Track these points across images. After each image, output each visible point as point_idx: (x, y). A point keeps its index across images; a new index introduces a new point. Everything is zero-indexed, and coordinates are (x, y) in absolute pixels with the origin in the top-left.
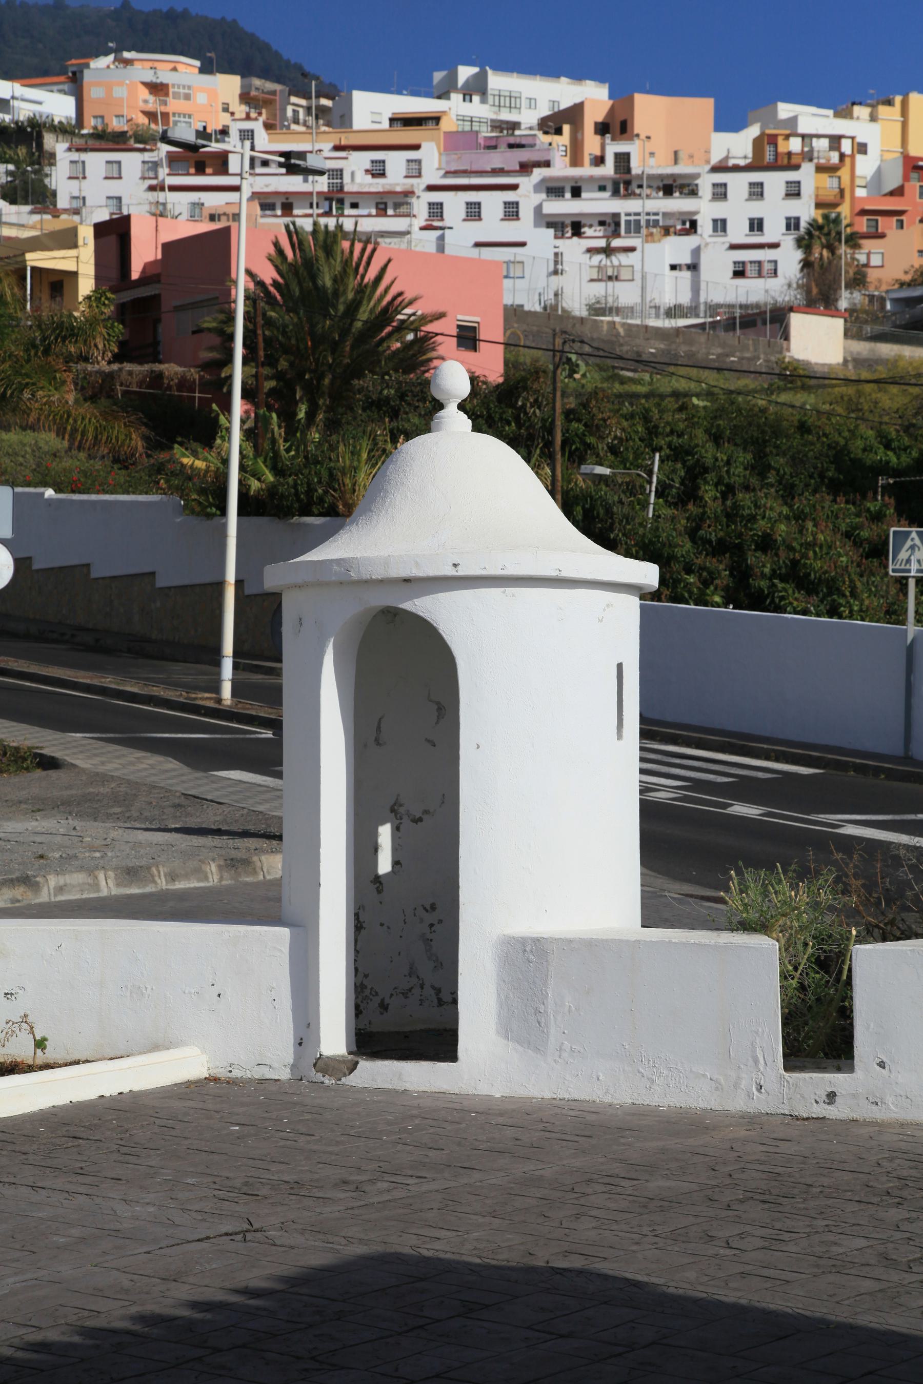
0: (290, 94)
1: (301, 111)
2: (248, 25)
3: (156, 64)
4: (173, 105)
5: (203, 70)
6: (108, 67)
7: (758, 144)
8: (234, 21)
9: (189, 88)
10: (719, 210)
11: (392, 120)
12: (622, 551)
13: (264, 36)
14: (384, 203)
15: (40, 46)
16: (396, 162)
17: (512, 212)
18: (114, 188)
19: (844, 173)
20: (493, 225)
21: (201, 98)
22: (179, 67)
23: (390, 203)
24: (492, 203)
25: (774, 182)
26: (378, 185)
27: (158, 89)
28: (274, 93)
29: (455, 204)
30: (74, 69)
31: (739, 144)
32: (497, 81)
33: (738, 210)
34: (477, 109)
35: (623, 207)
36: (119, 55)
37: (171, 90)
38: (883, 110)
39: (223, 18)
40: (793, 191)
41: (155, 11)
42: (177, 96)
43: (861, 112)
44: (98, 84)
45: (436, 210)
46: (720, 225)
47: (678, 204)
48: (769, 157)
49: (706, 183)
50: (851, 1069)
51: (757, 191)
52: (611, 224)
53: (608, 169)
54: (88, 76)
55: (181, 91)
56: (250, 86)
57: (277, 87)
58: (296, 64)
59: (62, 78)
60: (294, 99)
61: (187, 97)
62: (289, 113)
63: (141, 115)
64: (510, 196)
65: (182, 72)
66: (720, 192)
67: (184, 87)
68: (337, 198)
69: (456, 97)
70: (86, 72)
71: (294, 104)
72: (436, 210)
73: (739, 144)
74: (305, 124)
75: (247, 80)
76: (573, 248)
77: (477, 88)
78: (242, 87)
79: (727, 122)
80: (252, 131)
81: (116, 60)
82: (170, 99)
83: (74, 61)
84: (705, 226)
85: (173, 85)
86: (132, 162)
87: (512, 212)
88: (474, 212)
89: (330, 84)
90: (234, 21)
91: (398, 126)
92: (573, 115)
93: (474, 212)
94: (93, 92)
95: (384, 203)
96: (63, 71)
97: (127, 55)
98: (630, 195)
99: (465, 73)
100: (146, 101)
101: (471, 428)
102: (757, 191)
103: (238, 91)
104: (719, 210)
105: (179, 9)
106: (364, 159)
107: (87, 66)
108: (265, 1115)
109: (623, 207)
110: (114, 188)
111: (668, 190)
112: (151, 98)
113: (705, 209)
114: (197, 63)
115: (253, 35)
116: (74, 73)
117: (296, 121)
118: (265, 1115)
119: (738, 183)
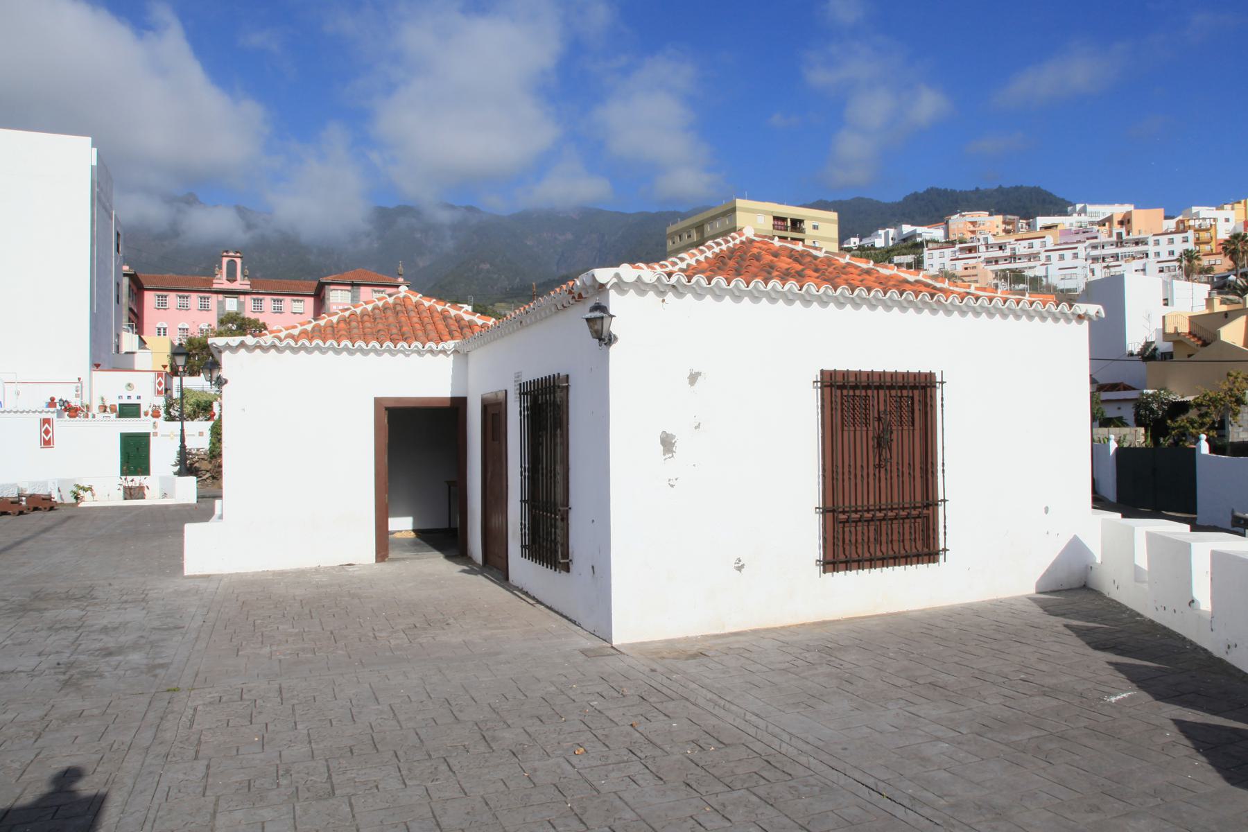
2: (1043, 188)
7: (1178, 223)
10: (1157, 249)
13: (1049, 190)
16: (1037, 243)
17: (1076, 256)
18: (942, 260)
19: (1212, 231)
20: (1069, 261)
23: (1033, 257)
24: (1068, 254)
25: (1178, 238)
26: (1030, 251)
31: (1171, 224)
32: (1090, 208)
34: (1083, 218)
38: (1236, 206)
43: (1228, 207)
45: (1048, 258)
46: (1157, 254)
47: (1141, 248)
48: (1181, 229)
49: (1151, 240)
50: (122, 434)
51: (1171, 241)
52: (1116, 257)
53: (1114, 238)
65: (982, 217)
66: (1157, 243)
68: (1014, 257)
69: (1075, 215)
72: (1048, 258)
73: (1171, 224)
77: (1084, 211)
84: (1151, 255)
87: (1076, 256)
88: (1062, 257)
92: (1109, 219)
93: (1062, 257)
94: (952, 226)
98: (1122, 246)
99: (1079, 206)
101: (830, 367)
104: (1157, 249)
106: (1026, 243)
110: (942, 260)
111: (1137, 244)
113: (1151, 249)
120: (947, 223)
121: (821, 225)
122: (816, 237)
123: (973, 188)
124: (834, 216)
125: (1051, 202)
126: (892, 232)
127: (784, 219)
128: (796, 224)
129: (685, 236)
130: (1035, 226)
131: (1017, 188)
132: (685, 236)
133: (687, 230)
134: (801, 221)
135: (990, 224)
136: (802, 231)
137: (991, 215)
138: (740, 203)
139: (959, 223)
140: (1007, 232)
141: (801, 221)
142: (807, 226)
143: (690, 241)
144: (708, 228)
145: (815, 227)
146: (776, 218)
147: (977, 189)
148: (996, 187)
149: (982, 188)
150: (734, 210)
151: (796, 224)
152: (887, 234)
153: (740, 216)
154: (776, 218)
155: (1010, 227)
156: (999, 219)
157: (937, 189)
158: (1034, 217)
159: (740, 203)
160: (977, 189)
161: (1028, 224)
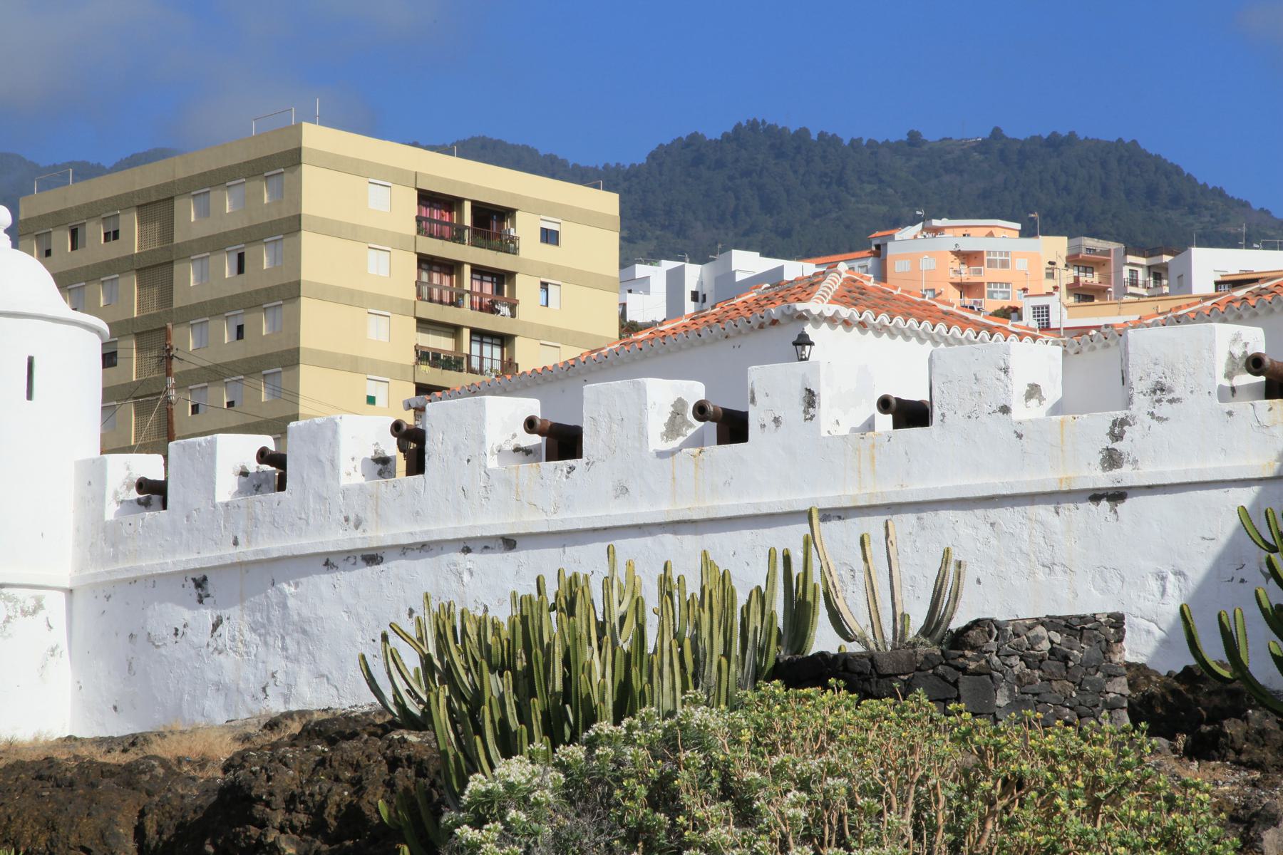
0: (1126, 254)
1: (1140, 271)
2: (1150, 146)
3: (970, 231)
4: (988, 275)
5: (1023, 234)
6: (915, 237)
8: (1134, 142)
9: (1007, 253)
11: (1217, 284)
13: (1171, 157)
15: (890, 191)
21: (1020, 264)
22: (994, 231)
27: (968, 257)
28: (1108, 253)
30: (878, 242)
36: (927, 223)
37: (986, 258)
39: (1120, 140)
41: (1033, 138)
42: (992, 264)
44: (902, 257)
54: (892, 249)
55: (998, 258)
56: (1080, 246)
57: (1112, 246)
58: (1215, 188)
59: (865, 253)
60: (1131, 259)
61: (1005, 264)
62: (1126, 274)
63: (952, 288)
65: (998, 237)
67: (1001, 253)
70: (889, 244)
71: (1131, 264)
74: (1145, 286)
75: (1075, 241)
78: (1070, 248)
80: (1047, 307)
81: (924, 229)
82: (985, 268)
83: (878, 234)
85: (989, 253)
89: (1262, 209)
90: (1134, 142)
91: (520, 455)
94: (898, 265)
96: (865, 245)
97: (936, 223)
100: (958, 272)
103: (1065, 253)
105: (1064, 133)
107: (892, 237)
112: (964, 268)
114: (1018, 226)
115: (1158, 157)
116: (878, 247)
117: (1134, 283)
120: (879, 252)
121: (567, 231)
122: (551, 269)
123: (898, 134)
124: (608, 203)
125: (1176, 201)
126: (694, 274)
127: (451, 203)
128: (491, 221)
129: (95, 232)
130: (1183, 282)
131: (1055, 143)
132: (95, 232)
133: (108, 211)
134: (506, 214)
135: (1028, 261)
136: (508, 245)
137: (1027, 232)
138: (315, 137)
139: (923, 254)
140: (1084, 295)
141: (506, 214)
142: (525, 228)
143: (114, 251)
144: (190, 218)
145: (549, 237)
146: (426, 198)
147: (914, 139)
148: (980, 132)
149: (931, 134)
150: (293, 158)
151: (491, 221)
152: (675, 280)
153: (311, 177)
154: (426, 198)
155: (1092, 279)
156: (1056, 247)
157: (771, 131)
158: (1179, 246)
159: (315, 137)
160: (914, 139)
161: (1157, 273)
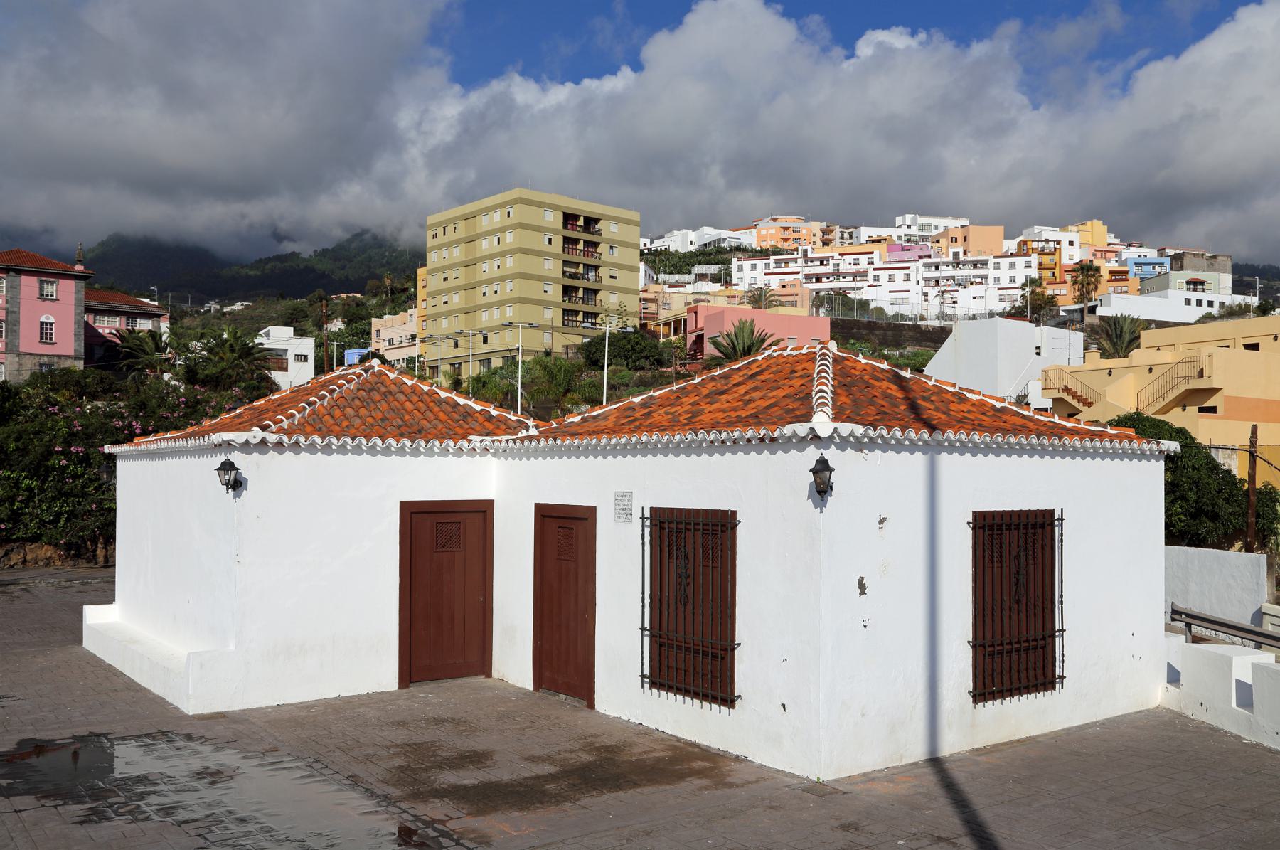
12: (110, 529)
14: (855, 276)
16: (863, 259)
17: (908, 278)
20: (899, 283)
21: (804, 232)
24: (899, 275)
25: (1020, 261)
29: (884, 275)
31: (1012, 245)
33: (1005, 273)
35: (957, 273)
40: (1028, 266)
45: (876, 278)
46: (997, 280)
49: (992, 261)
51: (1012, 266)
53: (950, 259)
64: (907, 271)
66: (997, 267)
72: (876, 278)
76: (933, 292)
79: (1008, 236)
86: (760, 264)
87: (908, 278)
93: (891, 279)
95: (855, 276)
102: (1012, 266)
106: (850, 259)
108: (228, 758)
109: (957, 273)
118: (228, 758)
119: (1005, 262)
